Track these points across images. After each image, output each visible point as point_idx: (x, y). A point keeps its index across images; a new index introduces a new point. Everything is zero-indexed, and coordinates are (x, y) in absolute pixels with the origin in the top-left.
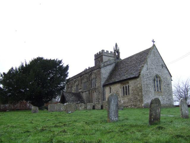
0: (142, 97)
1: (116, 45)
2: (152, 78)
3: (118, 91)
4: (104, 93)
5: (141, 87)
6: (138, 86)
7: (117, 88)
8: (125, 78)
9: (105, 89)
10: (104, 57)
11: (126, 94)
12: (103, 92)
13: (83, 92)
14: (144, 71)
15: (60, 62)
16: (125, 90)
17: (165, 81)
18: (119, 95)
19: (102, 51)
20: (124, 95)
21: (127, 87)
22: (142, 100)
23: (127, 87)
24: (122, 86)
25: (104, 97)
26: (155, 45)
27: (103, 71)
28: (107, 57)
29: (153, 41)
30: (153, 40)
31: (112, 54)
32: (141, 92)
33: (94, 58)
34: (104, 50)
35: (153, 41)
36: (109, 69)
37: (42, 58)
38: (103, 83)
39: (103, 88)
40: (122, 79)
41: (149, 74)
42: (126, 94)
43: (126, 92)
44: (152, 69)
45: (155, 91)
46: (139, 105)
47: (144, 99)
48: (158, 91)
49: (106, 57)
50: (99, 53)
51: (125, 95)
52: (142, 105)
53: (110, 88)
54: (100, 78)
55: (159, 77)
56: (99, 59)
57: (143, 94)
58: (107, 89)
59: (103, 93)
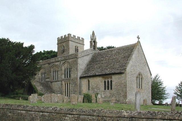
0: (126, 93)
1: (93, 34)
2: (135, 76)
3: (98, 85)
4: (81, 86)
5: (126, 83)
6: (123, 82)
7: (99, 82)
8: (107, 72)
9: (82, 81)
10: (70, 42)
11: (108, 89)
12: (80, 84)
13: (52, 82)
14: (129, 68)
15: (22, 44)
16: (107, 85)
17: (145, 79)
18: (99, 88)
19: (68, 34)
20: (105, 90)
21: (110, 83)
22: (126, 96)
23: (110, 83)
24: (104, 80)
25: (81, 90)
26: (140, 42)
27: (80, 61)
28: (73, 42)
29: (138, 38)
30: (138, 36)
31: (80, 40)
32: (126, 88)
33: (56, 42)
34: (71, 35)
35: (138, 38)
36: (87, 59)
37: (8, 40)
38: (80, 74)
39: (80, 80)
40: (104, 73)
41: (133, 71)
42: (108, 89)
43: (108, 86)
44: (135, 66)
45: (137, 88)
46: (122, 100)
47: (128, 95)
48: (139, 88)
49: (72, 42)
50: (61, 38)
51: (107, 89)
52: (126, 101)
53: (89, 81)
54: (77, 69)
55: (141, 75)
56: (64, 44)
57: (127, 90)
58: (85, 82)
59: (80, 85)
